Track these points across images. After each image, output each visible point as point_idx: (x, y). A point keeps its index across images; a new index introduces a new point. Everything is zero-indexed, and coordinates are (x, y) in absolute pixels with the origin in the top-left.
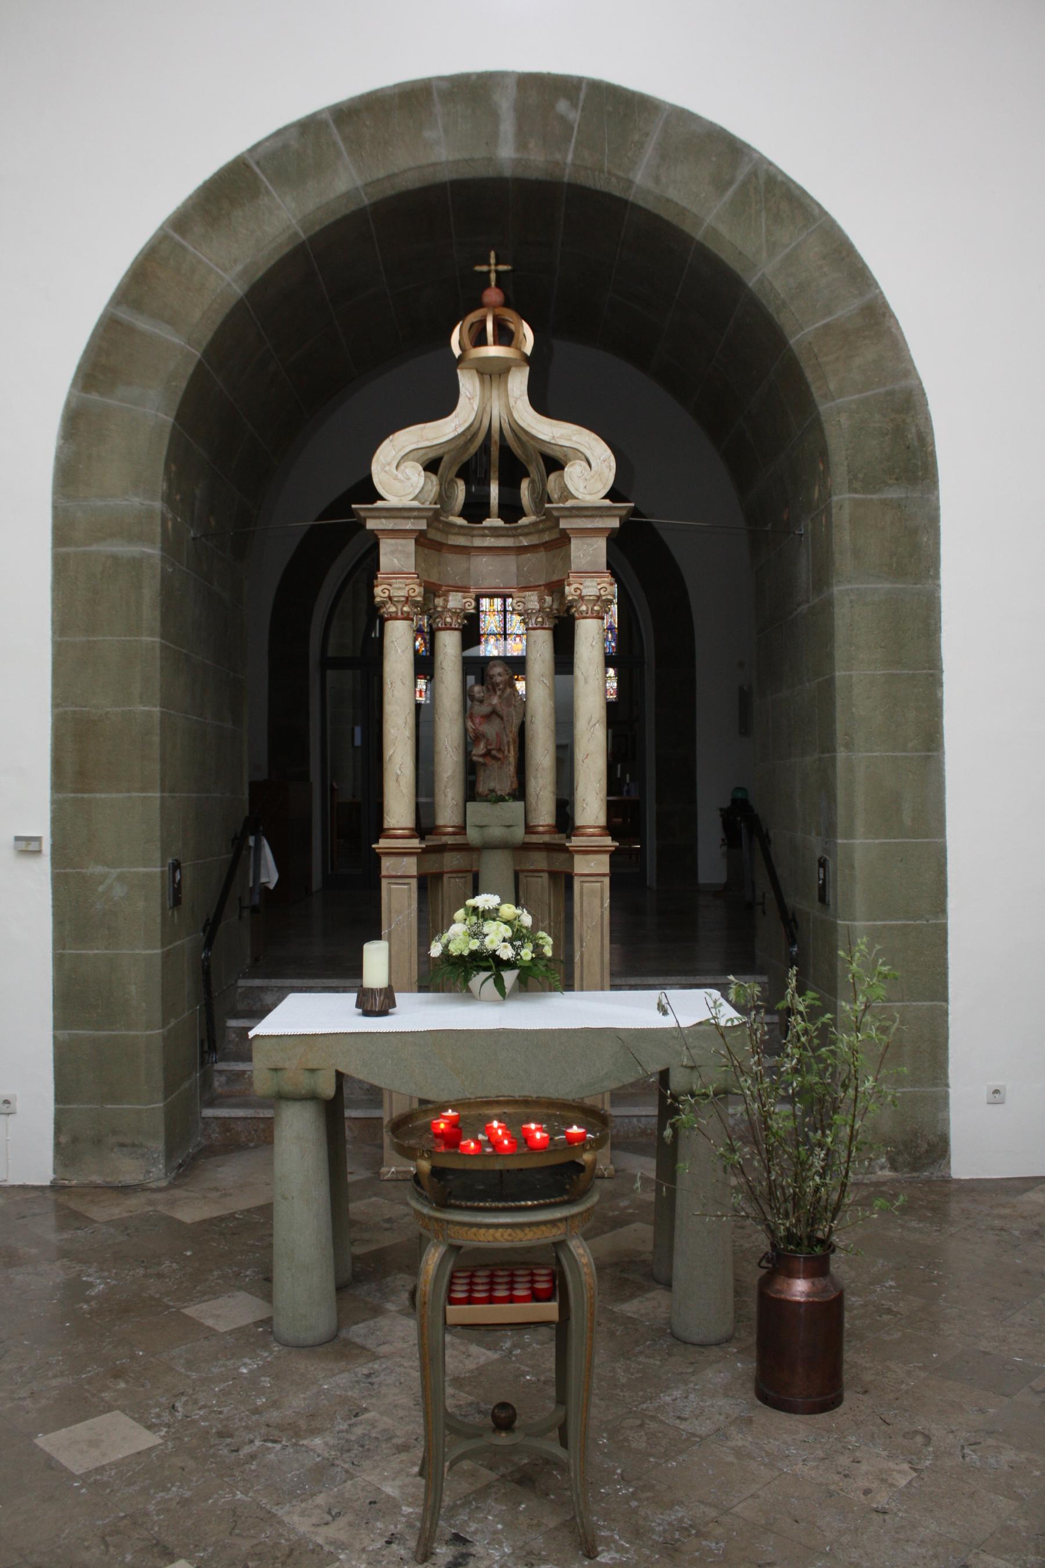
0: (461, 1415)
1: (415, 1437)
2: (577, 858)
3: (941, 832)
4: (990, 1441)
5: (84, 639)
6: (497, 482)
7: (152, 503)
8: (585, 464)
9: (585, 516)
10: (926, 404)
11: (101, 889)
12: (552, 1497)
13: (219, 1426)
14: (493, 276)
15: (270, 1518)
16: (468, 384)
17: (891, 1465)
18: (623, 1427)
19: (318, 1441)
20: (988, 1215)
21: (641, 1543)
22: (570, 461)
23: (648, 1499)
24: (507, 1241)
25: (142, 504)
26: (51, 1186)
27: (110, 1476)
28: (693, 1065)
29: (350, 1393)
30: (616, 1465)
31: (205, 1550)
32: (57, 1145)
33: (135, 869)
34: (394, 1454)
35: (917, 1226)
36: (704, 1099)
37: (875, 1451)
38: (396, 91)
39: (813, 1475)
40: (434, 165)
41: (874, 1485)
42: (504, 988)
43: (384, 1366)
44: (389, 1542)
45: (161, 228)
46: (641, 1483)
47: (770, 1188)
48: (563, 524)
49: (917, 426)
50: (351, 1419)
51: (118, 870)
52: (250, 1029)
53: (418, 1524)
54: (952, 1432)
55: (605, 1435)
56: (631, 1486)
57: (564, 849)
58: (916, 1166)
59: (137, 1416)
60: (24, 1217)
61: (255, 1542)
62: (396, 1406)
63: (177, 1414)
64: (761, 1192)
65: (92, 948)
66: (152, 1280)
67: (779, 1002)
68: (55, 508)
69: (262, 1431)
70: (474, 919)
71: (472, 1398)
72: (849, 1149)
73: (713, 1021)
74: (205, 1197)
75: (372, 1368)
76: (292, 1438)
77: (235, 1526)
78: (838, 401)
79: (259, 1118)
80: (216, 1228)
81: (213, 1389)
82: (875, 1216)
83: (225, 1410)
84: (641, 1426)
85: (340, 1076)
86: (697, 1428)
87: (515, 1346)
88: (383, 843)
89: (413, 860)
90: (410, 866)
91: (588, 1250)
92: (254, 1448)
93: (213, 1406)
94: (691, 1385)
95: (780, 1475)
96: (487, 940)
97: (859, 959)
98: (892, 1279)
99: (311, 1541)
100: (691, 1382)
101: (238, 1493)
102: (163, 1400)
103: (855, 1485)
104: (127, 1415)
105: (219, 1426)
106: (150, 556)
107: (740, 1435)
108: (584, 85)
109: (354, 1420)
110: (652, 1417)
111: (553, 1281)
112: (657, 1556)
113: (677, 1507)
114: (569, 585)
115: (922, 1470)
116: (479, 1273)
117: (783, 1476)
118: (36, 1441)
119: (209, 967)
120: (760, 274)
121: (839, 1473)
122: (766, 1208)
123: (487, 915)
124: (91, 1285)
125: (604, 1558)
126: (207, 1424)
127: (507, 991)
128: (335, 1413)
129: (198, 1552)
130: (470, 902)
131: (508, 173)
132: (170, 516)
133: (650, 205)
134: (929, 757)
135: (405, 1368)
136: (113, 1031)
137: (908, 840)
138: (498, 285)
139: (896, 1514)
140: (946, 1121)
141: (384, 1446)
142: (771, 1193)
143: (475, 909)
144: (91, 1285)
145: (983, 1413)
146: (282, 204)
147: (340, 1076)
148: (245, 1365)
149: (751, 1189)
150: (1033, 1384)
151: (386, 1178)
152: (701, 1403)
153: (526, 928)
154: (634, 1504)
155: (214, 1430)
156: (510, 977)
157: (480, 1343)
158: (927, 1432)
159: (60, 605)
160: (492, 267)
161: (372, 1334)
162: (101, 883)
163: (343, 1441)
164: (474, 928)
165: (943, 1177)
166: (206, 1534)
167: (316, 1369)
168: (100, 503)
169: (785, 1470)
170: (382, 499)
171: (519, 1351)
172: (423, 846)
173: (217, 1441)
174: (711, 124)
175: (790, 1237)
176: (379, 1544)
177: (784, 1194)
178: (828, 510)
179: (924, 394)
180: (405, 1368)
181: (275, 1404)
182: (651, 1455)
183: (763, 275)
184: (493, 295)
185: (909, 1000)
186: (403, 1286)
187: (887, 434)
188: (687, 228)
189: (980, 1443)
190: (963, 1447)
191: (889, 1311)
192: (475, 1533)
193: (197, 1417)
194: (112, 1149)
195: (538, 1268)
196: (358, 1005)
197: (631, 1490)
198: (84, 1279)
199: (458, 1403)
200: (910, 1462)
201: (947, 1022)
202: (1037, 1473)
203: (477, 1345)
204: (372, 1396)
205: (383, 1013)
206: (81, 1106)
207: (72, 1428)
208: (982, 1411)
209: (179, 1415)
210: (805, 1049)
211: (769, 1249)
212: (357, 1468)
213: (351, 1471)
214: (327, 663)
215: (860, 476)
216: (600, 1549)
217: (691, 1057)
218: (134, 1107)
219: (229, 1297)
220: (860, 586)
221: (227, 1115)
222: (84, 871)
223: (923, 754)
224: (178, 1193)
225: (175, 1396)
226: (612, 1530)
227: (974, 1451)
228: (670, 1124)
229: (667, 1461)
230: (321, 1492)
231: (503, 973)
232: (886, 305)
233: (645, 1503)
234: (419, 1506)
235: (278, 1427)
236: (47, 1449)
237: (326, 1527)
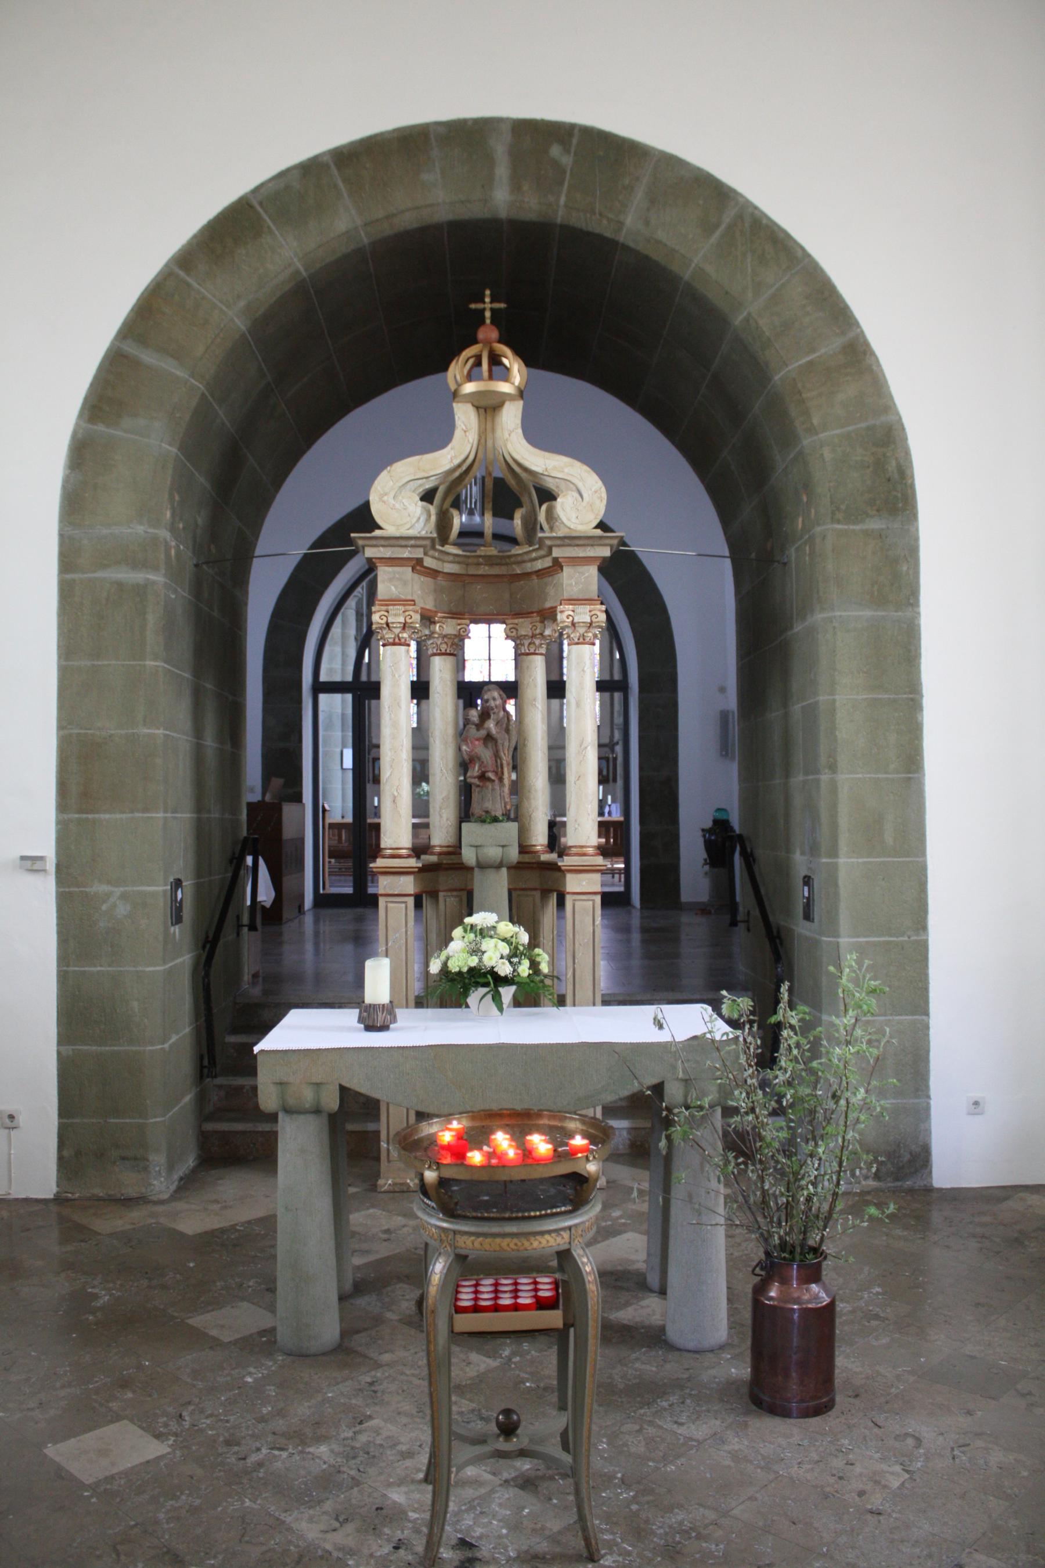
0: (463, 1421)
1: (418, 1444)
2: (569, 877)
3: (922, 851)
4: (979, 1443)
5: (89, 663)
6: (491, 513)
7: (156, 531)
8: (576, 495)
9: (577, 545)
10: (905, 439)
11: (104, 907)
12: (555, 1501)
13: (226, 1435)
14: (488, 314)
15: (279, 1524)
16: (465, 417)
17: (884, 1467)
18: (622, 1433)
19: (323, 1449)
20: (971, 1223)
21: (642, 1546)
22: (562, 492)
23: (648, 1502)
24: (513, 1250)
25: (146, 532)
26: (54, 1200)
27: (120, 1486)
28: (687, 1077)
29: (354, 1401)
30: (617, 1469)
31: (215, 1557)
32: (61, 1159)
33: (138, 888)
34: (399, 1461)
35: (901, 1234)
36: (698, 1112)
37: (868, 1453)
38: (395, 135)
39: (808, 1478)
40: (432, 205)
41: (869, 1487)
42: (502, 1004)
43: (387, 1374)
44: (396, 1548)
45: (167, 265)
46: (642, 1487)
47: (764, 1197)
48: (556, 553)
49: (897, 459)
50: (355, 1427)
51: (122, 889)
52: (256, 1044)
53: (425, 1530)
54: (942, 1434)
55: (604, 1440)
56: (632, 1490)
57: (558, 869)
58: (899, 1175)
59: (144, 1425)
60: (28, 1230)
61: (264, 1548)
62: (399, 1413)
63: (184, 1423)
64: (755, 1202)
65: (95, 966)
66: (156, 1292)
67: (771, 1016)
68: (61, 536)
69: (269, 1439)
70: (472, 936)
71: (474, 1405)
72: (841, 1158)
73: (708, 1036)
74: (206, 1209)
75: (375, 1376)
76: (298, 1445)
77: (244, 1534)
78: (821, 435)
79: (258, 1132)
80: (218, 1240)
81: (219, 1398)
82: (866, 1224)
83: (232, 1418)
84: (640, 1431)
85: (343, 1089)
86: (695, 1433)
87: (514, 1354)
88: (380, 863)
89: (410, 879)
90: (408, 884)
91: (591, 1259)
92: (261, 1456)
93: (220, 1414)
94: (687, 1391)
95: (776, 1478)
96: (485, 957)
97: (848, 975)
98: (879, 1286)
99: (319, 1547)
100: (687, 1387)
101: (247, 1500)
102: (170, 1409)
103: (850, 1487)
104: (135, 1424)
105: (226, 1435)
106: (154, 583)
107: (736, 1439)
108: (576, 131)
109: (358, 1428)
110: (650, 1421)
111: (556, 1289)
112: (659, 1559)
113: (676, 1510)
114: (562, 612)
115: (914, 1472)
116: (484, 1282)
117: (780, 1478)
118: (45, 1451)
119: (209, 984)
120: (745, 313)
121: (834, 1475)
122: (760, 1219)
123: (483, 933)
124: (96, 1297)
125: (607, 1561)
126: (214, 1432)
127: (505, 1006)
128: (339, 1421)
129: (209, 1559)
130: (468, 920)
131: (503, 214)
132: (173, 544)
133: (640, 247)
134: (910, 778)
135: (407, 1375)
136: (115, 1046)
137: (889, 859)
138: (493, 322)
139: (890, 1515)
140: (928, 1132)
141: (389, 1453)
142: (764, 1202)
143: (472, 927)
144: (96, 1297)
145: (971, 1415)
146: (283, 243)
147: (343, 1089)
148: (250, 1374)
149: (746, 1199)
150: (1019, 1387)
151: (383, 1190)
152: (697, 1408)
153: (523, 945)
154: (634, 1507)
155: (221, 1439)
156: (507, 993)
157: (479, 1351)
158: (917, 1435)
159: (66, 630)
160: (488, 305)
161: (374, 1343)
162: (104, 902)
163: (349, 1448)
164: (473, 946)
165: (925, 1186)
166: (216, 1541)
167: (319, 1378)
168: (105, 531)
169: (781, 1473)
170: (380, 528)
171: (518, 1359)
172: (420, 865)
173: (225, 1450)
174: (699, 170)
175: (783, 1245)
176: (387, 1549)
177: (777, 1204)
178: (811, 540)
179: (903, 429)
180: (407, 1375)
181: (281, 1413)
182: (650, 1460)
183: (749, 314)
184: (488, 332)
185: (892, 1015)
186: (403, 1295)
187: (868, 467)
188: (675, 267)
189: (969, 1445)
190: (952, 1449)
191: (877, 1317)
192: (480, 1538)
193: (204, 1425)
194: (115, 1163)
195: (541, 1277)
196: (361, 1020)
197: (631, 1494)
198: (90, 1290)
199: (460, 1410)
200: (901, 1464)
201: (928, 1035)
202: (1025, 1474)
203: (477, 1353)
204: (376, 1404)
205: (384, 1028)
206: (85, 1120)
207: (82, 1437)
208: (969, 1413)
209: (187, 1425)
210: (797, 1062)
211: (763, 1257)
212: (363, 1475)
213: (357, 1477)
214: (320, 687)
215: (843, 507)
216: (603, 1552)
217: (685, 1071)
218: (136, 1121)
219: (233, 1307)
220: (843, 614)
221: (226, 1129)
222: (87, 890)
223: (904, 775)
224: (180, 1205)
225: (182, 1405)
226: (613, 1533)
227: (963, 1452)
228: (666, 1135)
229: (665, 1465)
230: (328, 1499)
231: (500, 989)
232: (867, 344)
233: (646, 1506)
234: (424, 1511)
235: (283, 1435)
236: (57, 1459)
237: (335, 1533)
